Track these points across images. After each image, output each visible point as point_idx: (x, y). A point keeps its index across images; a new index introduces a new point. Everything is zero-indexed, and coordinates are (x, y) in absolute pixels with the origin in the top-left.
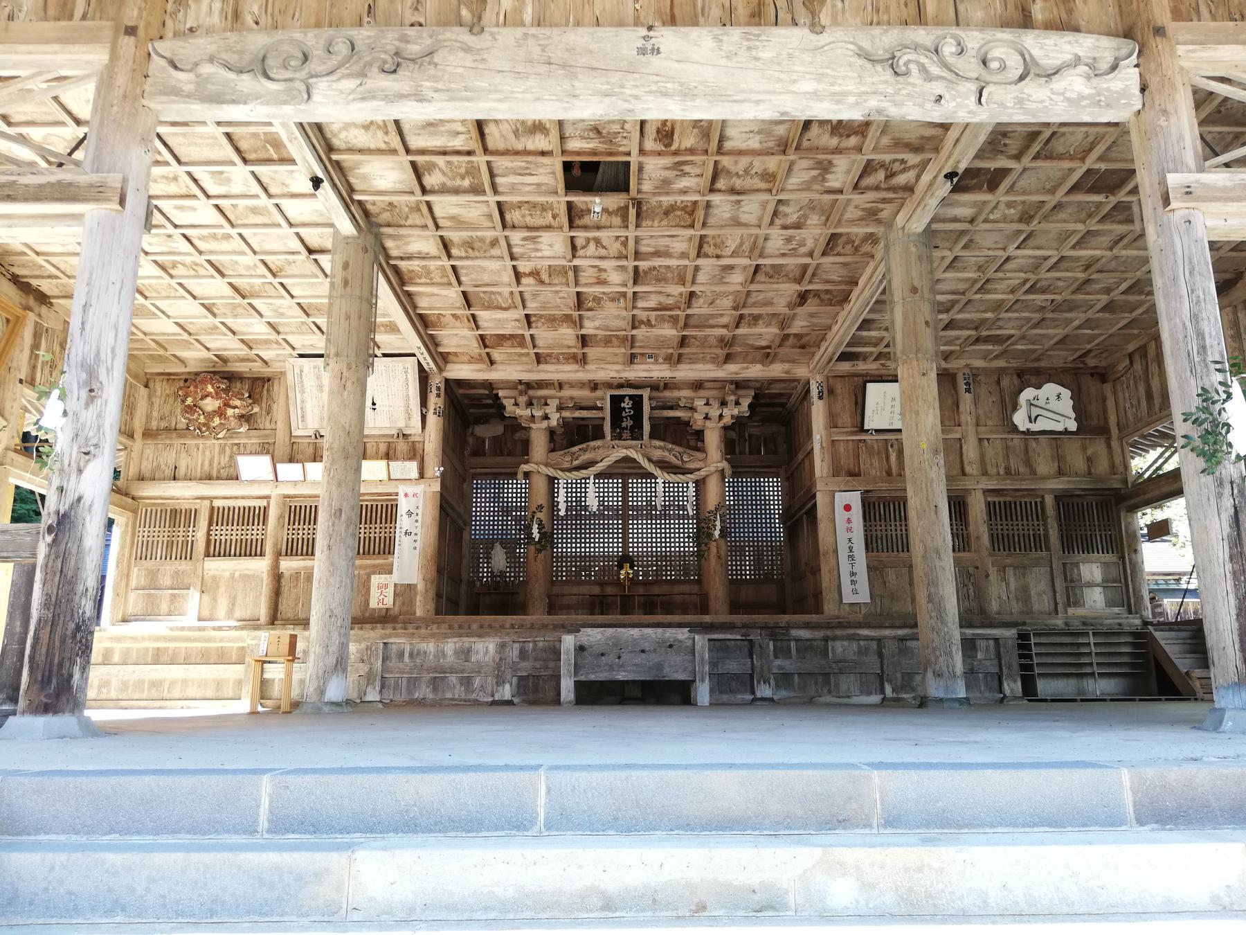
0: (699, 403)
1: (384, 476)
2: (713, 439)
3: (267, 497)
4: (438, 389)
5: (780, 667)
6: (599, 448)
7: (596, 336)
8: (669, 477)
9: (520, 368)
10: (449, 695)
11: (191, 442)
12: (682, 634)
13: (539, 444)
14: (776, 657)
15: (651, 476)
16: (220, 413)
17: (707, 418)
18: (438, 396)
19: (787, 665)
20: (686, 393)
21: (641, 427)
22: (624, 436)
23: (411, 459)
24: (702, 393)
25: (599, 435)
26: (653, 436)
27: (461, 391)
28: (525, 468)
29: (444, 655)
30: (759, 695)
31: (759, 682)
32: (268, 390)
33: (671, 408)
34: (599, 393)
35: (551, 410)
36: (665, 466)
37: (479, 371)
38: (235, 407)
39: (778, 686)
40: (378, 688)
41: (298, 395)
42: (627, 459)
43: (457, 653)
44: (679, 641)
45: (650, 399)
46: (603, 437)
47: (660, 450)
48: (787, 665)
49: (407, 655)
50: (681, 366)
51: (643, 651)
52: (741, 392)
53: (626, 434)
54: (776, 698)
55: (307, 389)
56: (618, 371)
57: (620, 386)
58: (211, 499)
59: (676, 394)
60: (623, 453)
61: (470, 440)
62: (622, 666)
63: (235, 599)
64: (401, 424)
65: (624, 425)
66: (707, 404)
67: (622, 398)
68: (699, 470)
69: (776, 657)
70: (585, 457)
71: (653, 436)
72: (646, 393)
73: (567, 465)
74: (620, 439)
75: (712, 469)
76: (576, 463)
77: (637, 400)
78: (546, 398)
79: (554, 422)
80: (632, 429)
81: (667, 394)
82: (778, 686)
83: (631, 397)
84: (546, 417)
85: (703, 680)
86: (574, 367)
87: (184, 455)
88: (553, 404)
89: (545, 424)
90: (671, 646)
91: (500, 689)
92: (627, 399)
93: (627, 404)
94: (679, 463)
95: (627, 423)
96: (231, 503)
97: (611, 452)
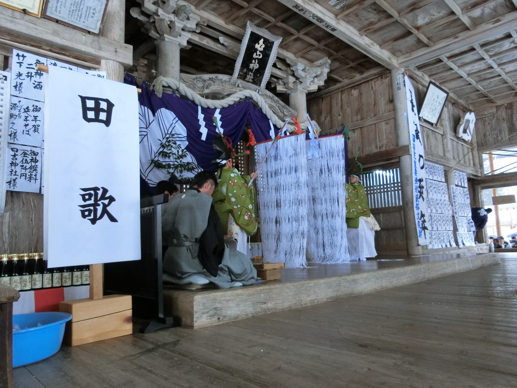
83: (266, 41)
92: (261, 41)
93: (260, 46)
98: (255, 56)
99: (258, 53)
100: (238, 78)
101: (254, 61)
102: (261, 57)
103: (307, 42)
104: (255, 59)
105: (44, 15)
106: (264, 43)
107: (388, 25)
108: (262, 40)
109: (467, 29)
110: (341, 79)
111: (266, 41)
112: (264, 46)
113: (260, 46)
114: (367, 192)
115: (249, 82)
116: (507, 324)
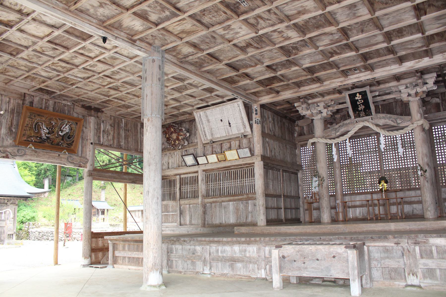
0: (402, 88)
1: (237, 157)
2: (415, 107)
3: (197, 172)
4: (256, 110)
5: (425, 264)
6: (349, 123)
7: (314, 66)
8: (387, 134)
9: (291, 91)
10: (238, 273)
11: (172, 152)
12: (341, 249)
13: (318, 127)
14: (422, 257)
15: (378, 134)
16: (178, 139)
17: (409, 95)
18: (256, 114)
19: (431, 263)
20: (394, 83)
21: (369, 108)
22: (361, 115)
23: (213, 154)
24: (403, 82)
25: (347, 116)
26: (377, 111)
27: (278, 108)
28: (311, 141)
29: (235, 253)
30: (409, 283)
31: (409, 274)
32: (194, 125)
33: (389, 94)
34: (343, 94)
35: (321, 108)
36: (386, 127)
37: (273, 97)
38: (182, 135)
39: (425, 277)
40: (209, 268)
41: (201, 126)
42: (364, 128)
43: (240, 251)
44: (340, 254)
45: (371, 92)
46: (349, 117)
47: (384, 119)
48: (431, 263)
49: (220, 252)
50: (376, 71)
51: (318, 260)
52: (426, 76)
53: (362, 114)
54: (422, 285)
55: (204, 122)
56: (341, 82)
57: (353, 88)
58: (180, 175)
59: (387, 85)
60: (360, 125)
61: (297, 128)
62: (306, 268)
63: (191, 216)
64: (242, 131)
65: (360, 109)
66: (407, 87)
67: (355, 95)
68: (407, 126)
69: (422, 257)
70: (343, 130)
71: (377, 111)
72: (367, 89)
73: (333, 136)
74: (359, 117)
75: (415, 125)
76: (338, 134)
77: (364, 94)
78: (317, 103)
79: (324, 114)
80: (365, 110)
81: (382, 86)
82: (425, 277)
83: (360, 93)
84: (320, 112)
85: (354, 280)
86: (318, 85)
87: (170, 158)
88: (322, 105)
89: (319, 116)
90: (334, 257)
91: (260, 271)
92: (358, 95)
93: (358, 97)
94: (395, 124)
95: (362, 107)
96: (186, 176)
97: (355, 125)
98: (358, 103)
99: (359, 101)
100: (355, 118)
101: (359, 106)
102: (363, 101)
103: (164, 22)
104: (360, 104)
105: (240, 158)
106: (359, 94)
107: (433, 120)
108: (358, 94)
109: (436, 246)
110: (63, 34)
111: (360, 93)
112: (361, 96)
113: (358, 97)
114: (418, 181)
115: (363, 117)
116: (441, 121)
